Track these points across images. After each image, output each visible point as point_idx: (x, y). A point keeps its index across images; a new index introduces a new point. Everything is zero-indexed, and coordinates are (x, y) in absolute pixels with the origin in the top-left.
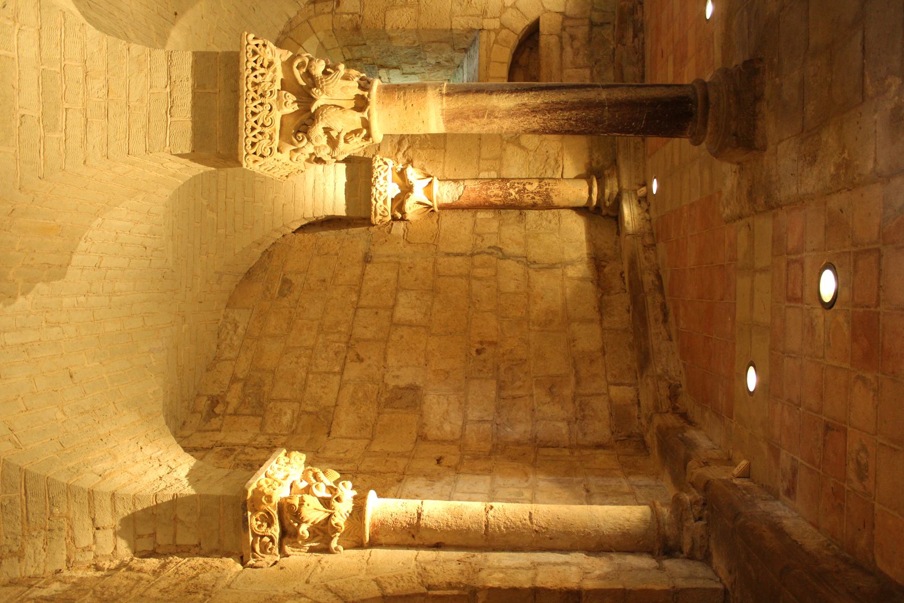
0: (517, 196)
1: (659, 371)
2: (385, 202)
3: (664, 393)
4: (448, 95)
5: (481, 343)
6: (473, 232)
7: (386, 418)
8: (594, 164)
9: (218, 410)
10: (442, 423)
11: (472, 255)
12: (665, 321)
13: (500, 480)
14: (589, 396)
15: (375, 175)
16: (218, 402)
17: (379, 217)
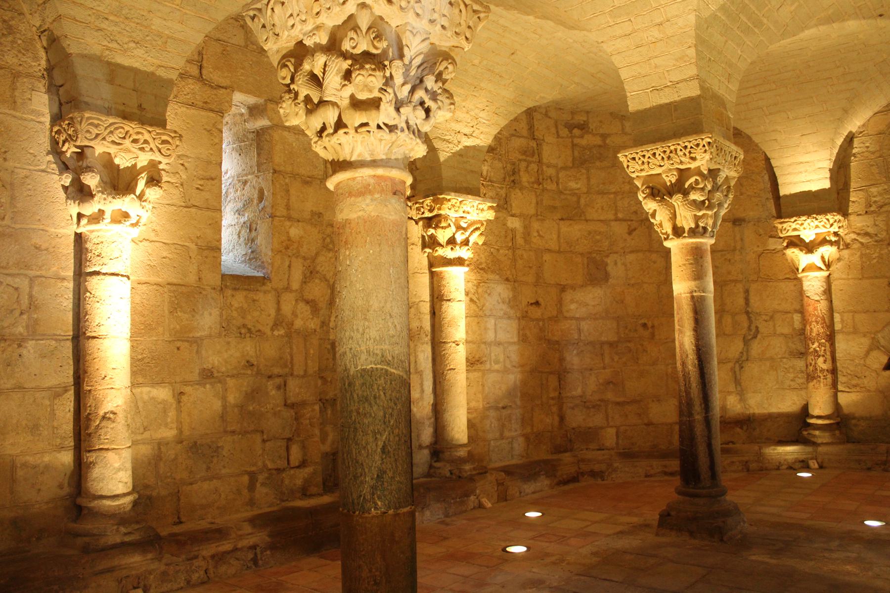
0: (812, 350)
1: (615, 465)
2: (795, 229)
3: (596, 467)
4: (692, 297)
5: (653, 327)
6: (776, 312)
7: (579, 259)
8: (853, 422)
9: (576, 132)
10: (577, 302)
11: (747, 313)
12: (666, 473)
13: (514, 348)
14: (606, 411)
15: (819, 217)
16: (582, 129)
17: (780, 226)
